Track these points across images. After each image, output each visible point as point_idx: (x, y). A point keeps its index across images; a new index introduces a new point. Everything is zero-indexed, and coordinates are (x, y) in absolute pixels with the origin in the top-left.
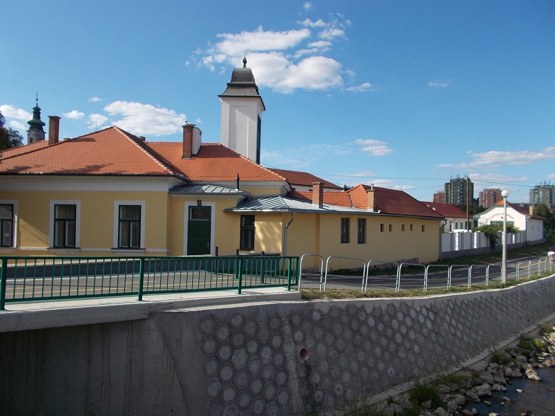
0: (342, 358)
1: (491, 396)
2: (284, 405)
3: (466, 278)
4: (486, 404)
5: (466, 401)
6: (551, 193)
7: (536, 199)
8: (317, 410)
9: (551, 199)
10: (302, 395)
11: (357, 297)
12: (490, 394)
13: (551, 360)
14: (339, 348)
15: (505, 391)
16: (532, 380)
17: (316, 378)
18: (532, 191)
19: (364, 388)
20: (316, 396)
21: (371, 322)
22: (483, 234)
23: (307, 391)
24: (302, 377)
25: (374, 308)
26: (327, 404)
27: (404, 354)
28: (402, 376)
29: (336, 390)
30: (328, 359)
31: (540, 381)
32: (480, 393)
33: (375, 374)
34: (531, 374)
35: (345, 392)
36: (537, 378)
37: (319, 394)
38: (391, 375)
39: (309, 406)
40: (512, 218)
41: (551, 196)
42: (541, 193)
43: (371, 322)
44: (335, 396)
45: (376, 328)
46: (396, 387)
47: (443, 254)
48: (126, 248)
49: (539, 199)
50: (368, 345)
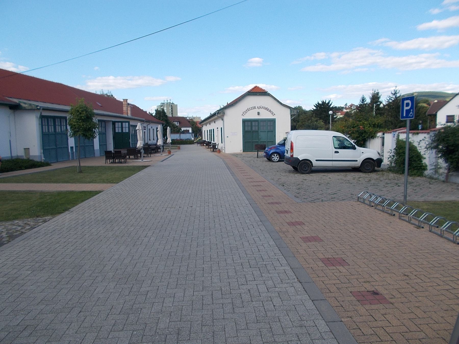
6: (172, 108)
18: (159, 107)
41: (172, 111)
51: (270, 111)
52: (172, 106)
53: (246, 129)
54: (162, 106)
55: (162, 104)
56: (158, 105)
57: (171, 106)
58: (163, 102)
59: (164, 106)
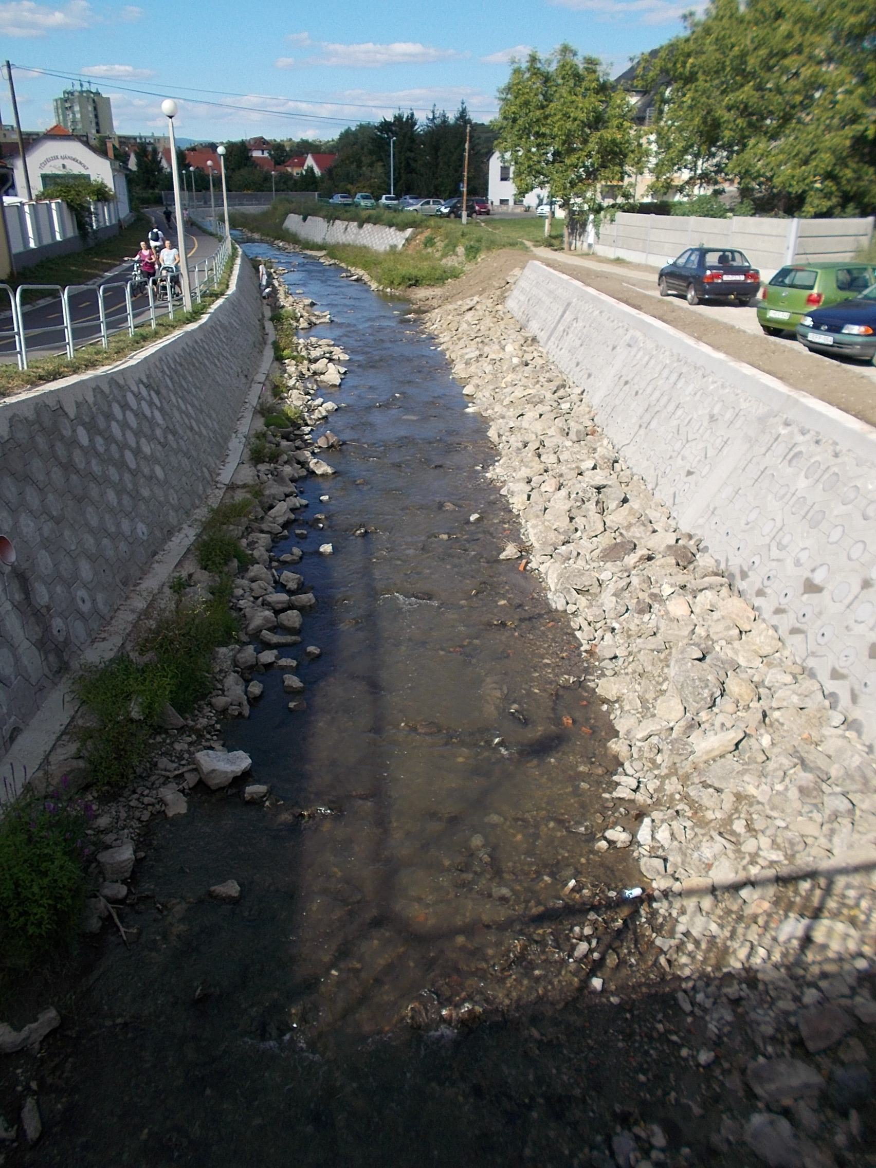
0: (67, 533)
1: (295, 520)
2: (13, 677)
3: (7, 313)
4: (298, 535)
5: (273, 541)
6: (95, 109)
7: (69, 124)
8: (66, 658)
9: (97, 124)
10: (34, 641)
11: (34, 385)
12: (293, 516)
13: (327, 438)
14: (55, 513)
15: (307, 506)
16: (322, 475)
17: (42, 595)
18: (59, 102)
19: (117, 580)
20: (55, 632)
21: (83, 436)
22: (65, 206)
23: (37, 629)
24: (19, 602)
25: (76, 402)
26: (77, 637)
27: (148, 489)
28: (158, 534)
29: (80, 603)
30: (46, 544)
31: (333, 473)
32: (281, 520)
33: (123, 546)
34: (319, 468)
35: (94, 601)
36: (329, 470)
37: (57, 623)
38: (145, 538)
39: (52, 658)
40: (84, 166)
41: (96, 116)
42: (77, 108)
43: (83, 436)
44: (82, 616)
45: (94, 448)
46: (156, 557)
47: (15, 259)
48: (628, 283)
49: (74, 122)
50: (94, 491)
51: (80, 163)
52: (94, 101)
53: (159, 211)
54: (66, 101)
55: (68, 93)
56: (56, 97)
57: (91, 101)
58: (70, 88)
59: (72, 102)
